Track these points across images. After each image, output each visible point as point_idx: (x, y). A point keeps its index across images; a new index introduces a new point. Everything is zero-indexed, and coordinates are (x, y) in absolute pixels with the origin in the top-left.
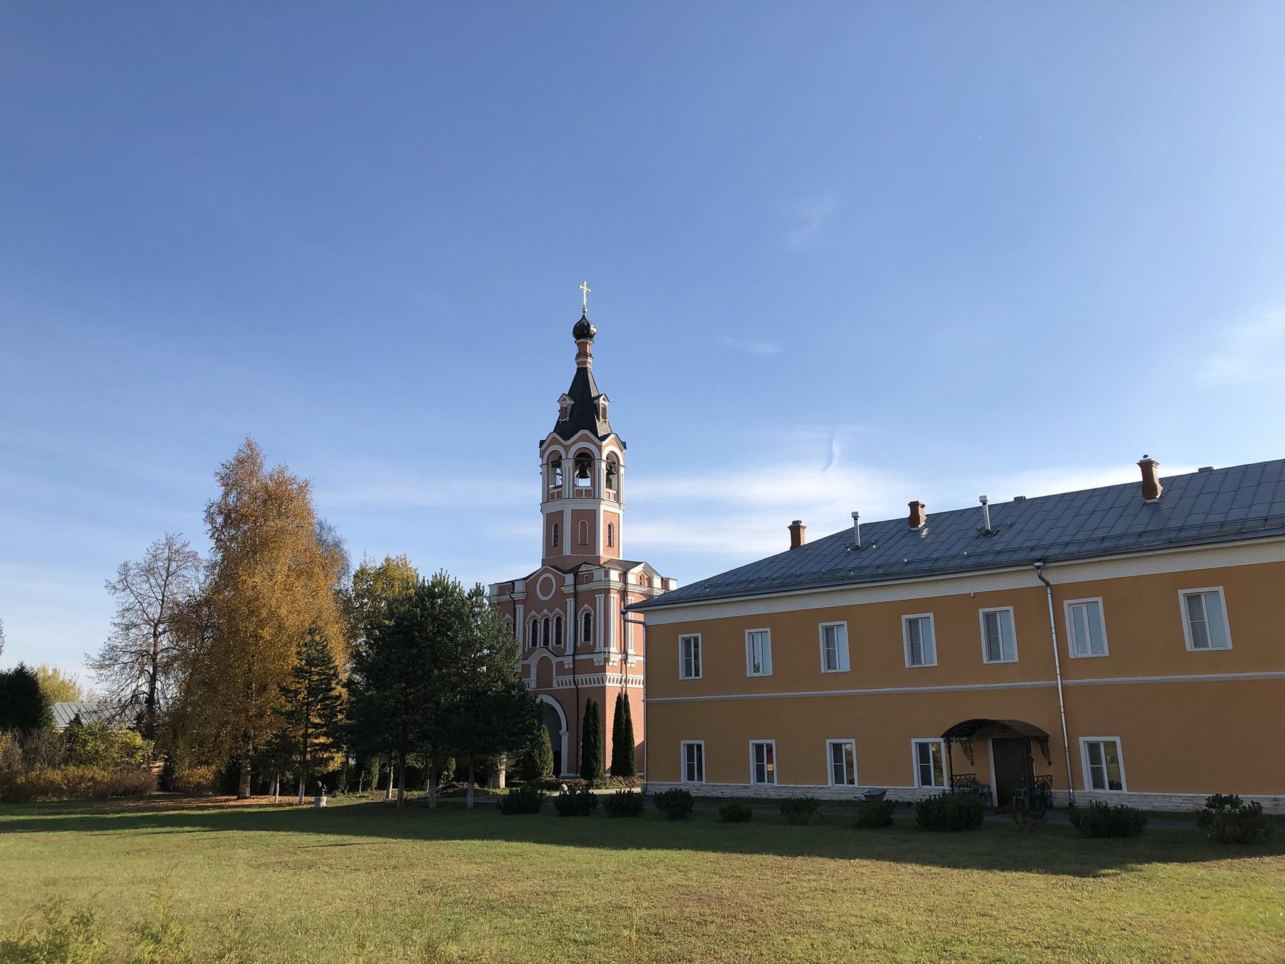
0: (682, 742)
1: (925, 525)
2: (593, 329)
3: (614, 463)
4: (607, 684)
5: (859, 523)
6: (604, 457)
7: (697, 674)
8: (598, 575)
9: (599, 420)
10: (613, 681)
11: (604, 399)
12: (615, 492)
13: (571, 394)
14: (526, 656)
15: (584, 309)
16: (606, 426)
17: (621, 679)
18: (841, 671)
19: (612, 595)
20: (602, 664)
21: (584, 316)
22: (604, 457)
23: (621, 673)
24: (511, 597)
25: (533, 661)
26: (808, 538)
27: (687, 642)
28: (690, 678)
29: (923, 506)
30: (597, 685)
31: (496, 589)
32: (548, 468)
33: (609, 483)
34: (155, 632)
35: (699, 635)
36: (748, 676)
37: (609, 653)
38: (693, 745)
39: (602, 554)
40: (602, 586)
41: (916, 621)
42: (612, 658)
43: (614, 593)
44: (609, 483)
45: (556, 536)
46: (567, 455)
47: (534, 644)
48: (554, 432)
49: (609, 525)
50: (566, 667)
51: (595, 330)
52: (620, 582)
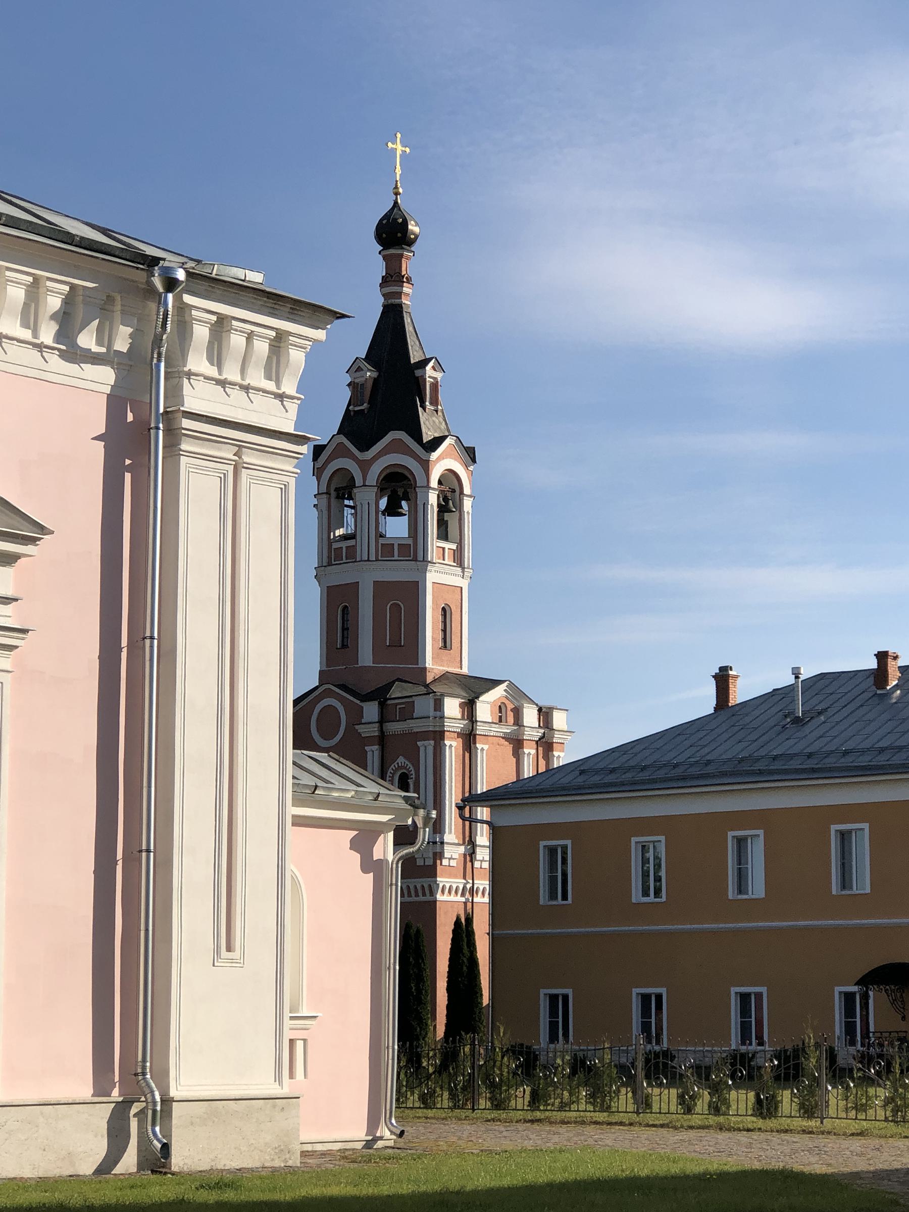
0: (543, 992)
1: (897, 685)
2: (413, 227)
3: (453, 491)
4: (439, 897)
5: (802, 677)
6: (434, 483)
7: (565, 897)
8: (423, 706)
9: (424, 409)
10: (450, 892)
11: (433, 367)
12: (454, 547)
13: (373, 356)
15: (396, 187)
16: (437, 420)
17: (464, 888)
18: (753, 897)
19: (447, 742)
20: (429, 862)
21: (396, 203)
22: (434, 483)
23: (464, 878)
26: (740, 693)
27: (552, 851)
28: (554, 903)
29: (896, 658)
30: (421, 898)
32: (329, 499)
33: (443, 527)
34: (905, 1100)
35: (569, 843)
36: (634, 900)
37: (442, 843)
38: (749, 995)
39: (429, 663)
40: (430, 726)
41: (850, 832)
42: (449, 851)
43: (451, 739)
44: (443, 527)
45: (345, 629)
46: (364, 478)
48: (338, 433)
49: (444, 609)
51: (416, 230)
52: (463, 718)
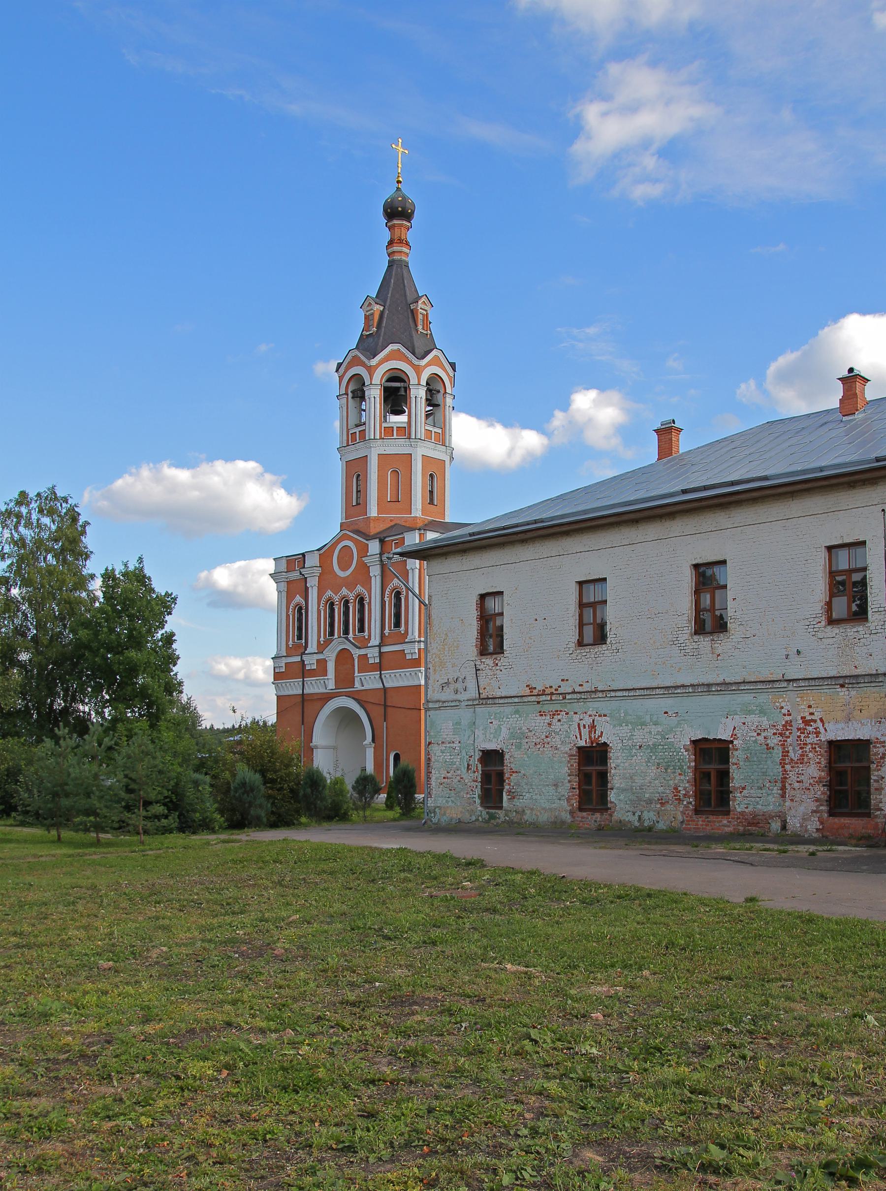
14: (321, 648)
24: (301, 574)
25: (330, 654)
31: (284, 561)
32: (347, 398)
46: (371, 379)
47: (332, 633)
50: (371, 661)
